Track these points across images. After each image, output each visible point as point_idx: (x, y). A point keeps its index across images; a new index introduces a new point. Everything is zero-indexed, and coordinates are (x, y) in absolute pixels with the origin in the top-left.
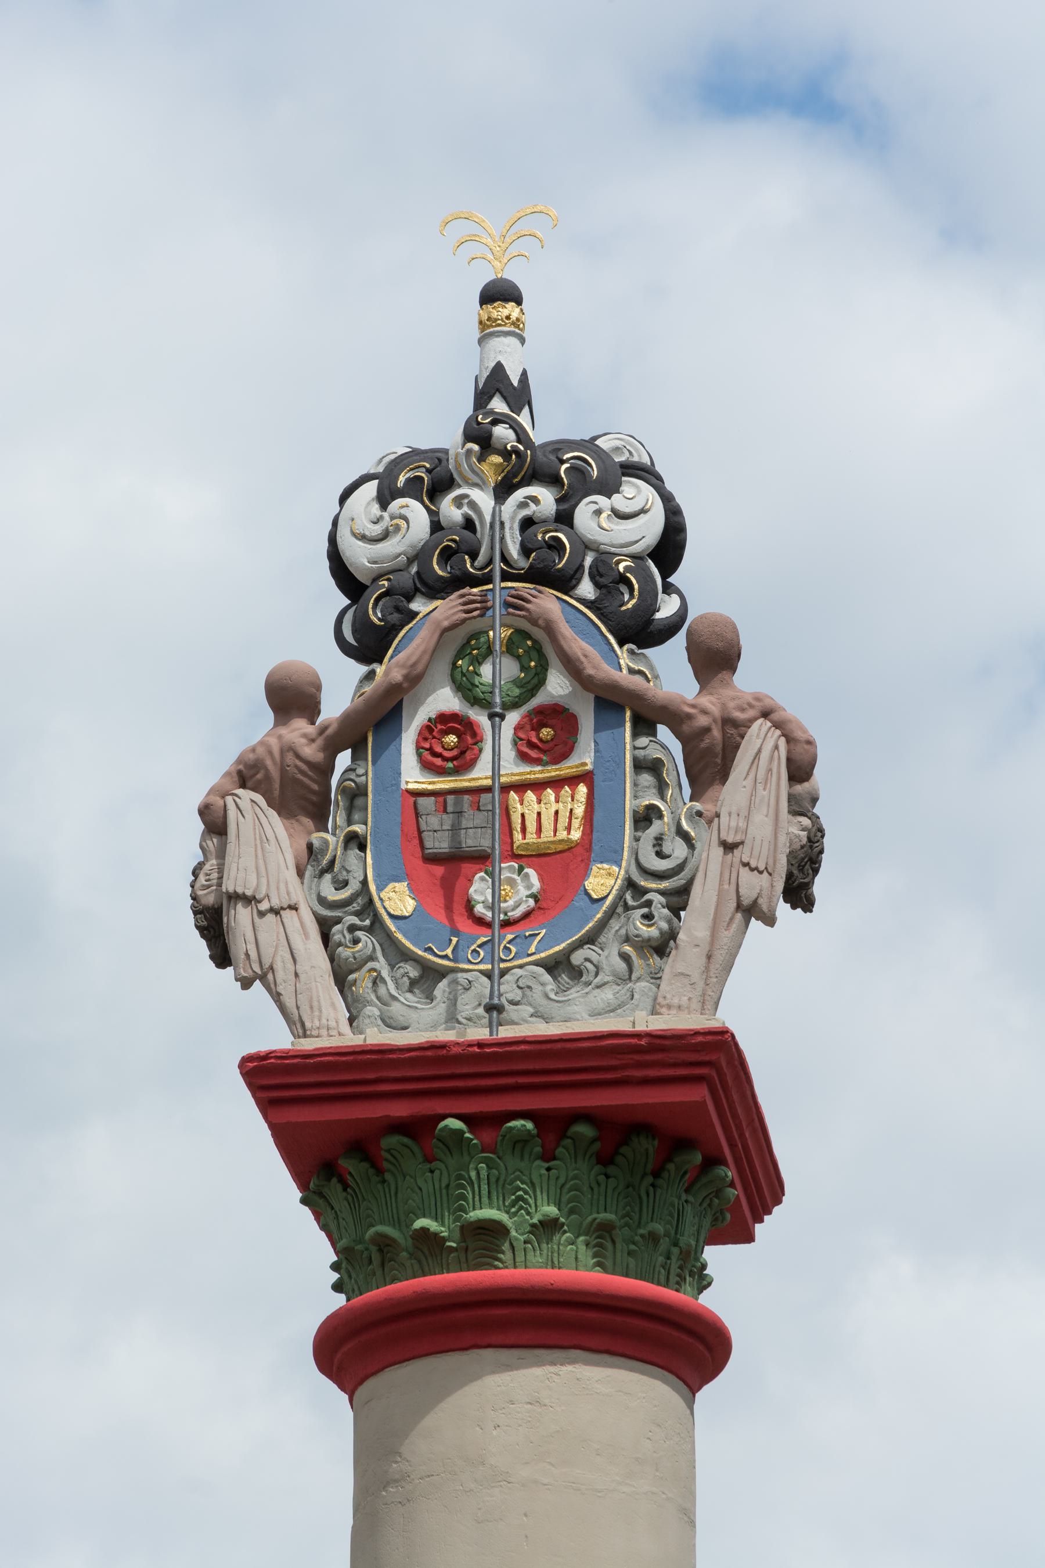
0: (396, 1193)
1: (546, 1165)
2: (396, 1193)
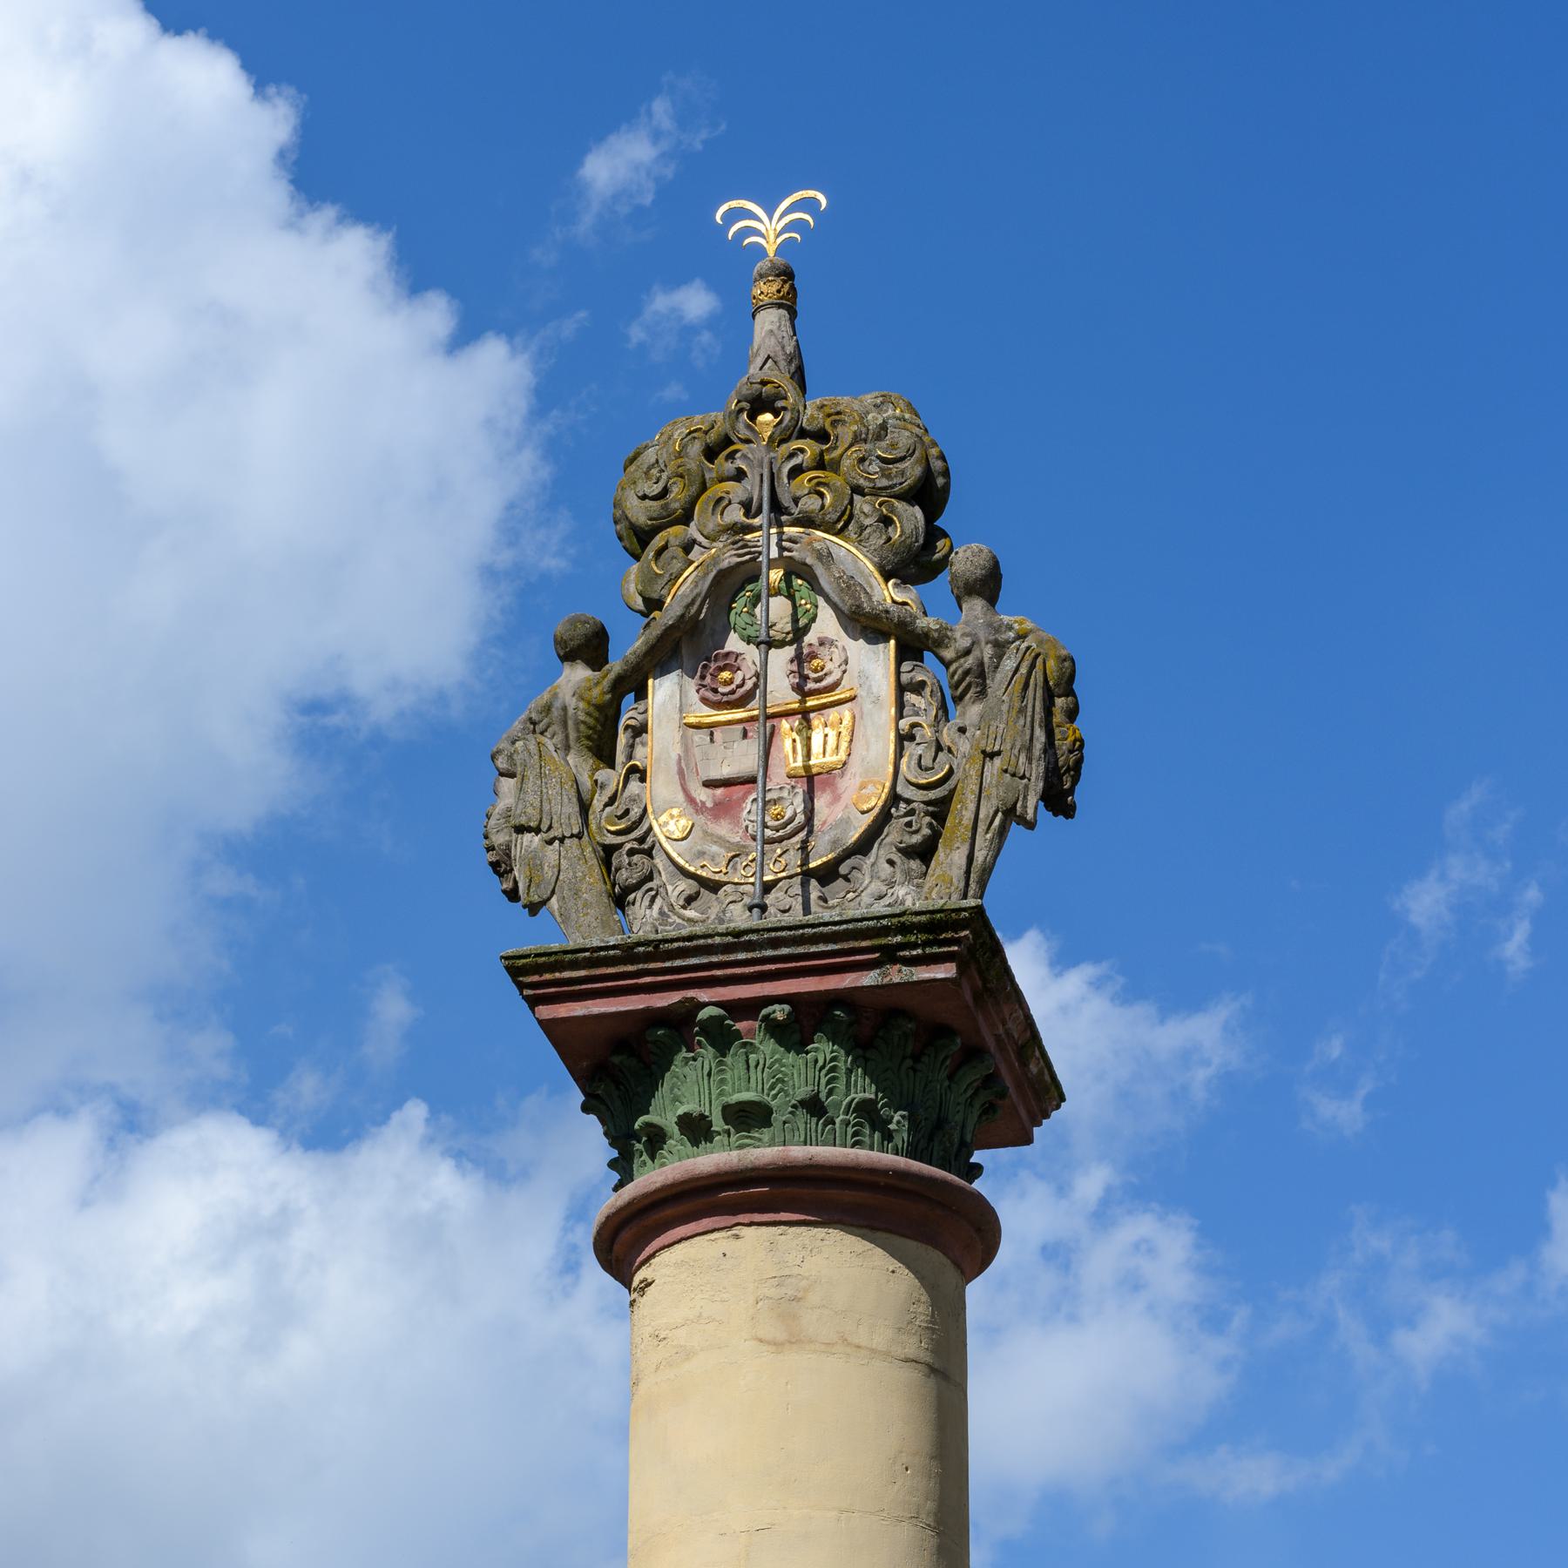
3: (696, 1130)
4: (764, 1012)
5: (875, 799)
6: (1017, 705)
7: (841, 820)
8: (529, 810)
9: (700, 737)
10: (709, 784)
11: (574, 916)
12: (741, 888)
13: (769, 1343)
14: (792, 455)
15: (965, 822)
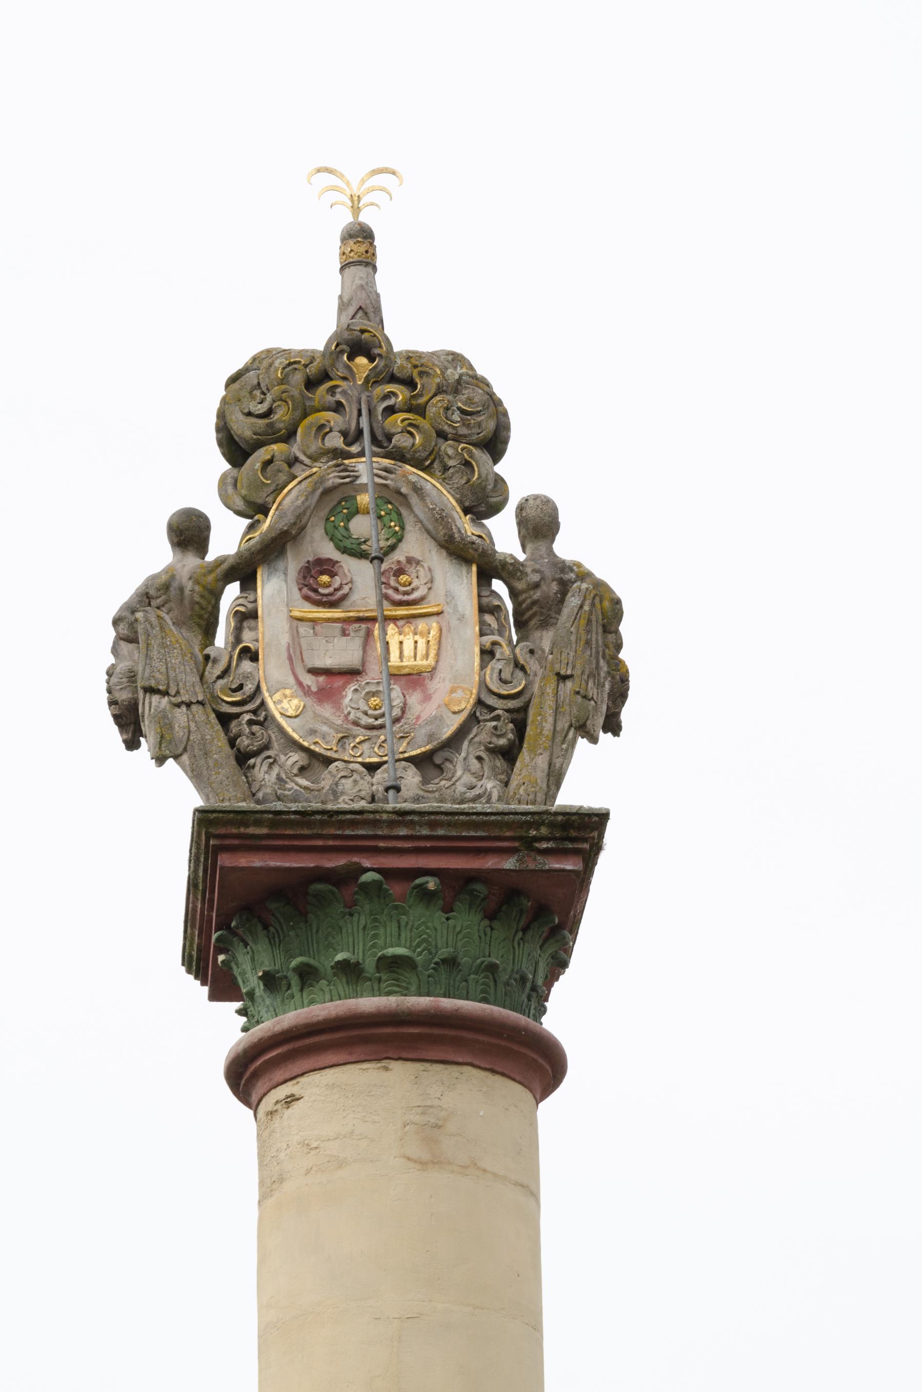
0: (317, 932)
1: (446, 916)
2: (317, 932)
3: (350, 972)
4: (418, 881)
5: (466, 703)
6: (584, 637)
7: (435, 717)
8: (158, 675)
9: (304, 629)
10: (315, 671)
11: (205, 772)
12: (351, 766)
13: (415, 1161)
14: (387, 396)
15: (545, 732)
